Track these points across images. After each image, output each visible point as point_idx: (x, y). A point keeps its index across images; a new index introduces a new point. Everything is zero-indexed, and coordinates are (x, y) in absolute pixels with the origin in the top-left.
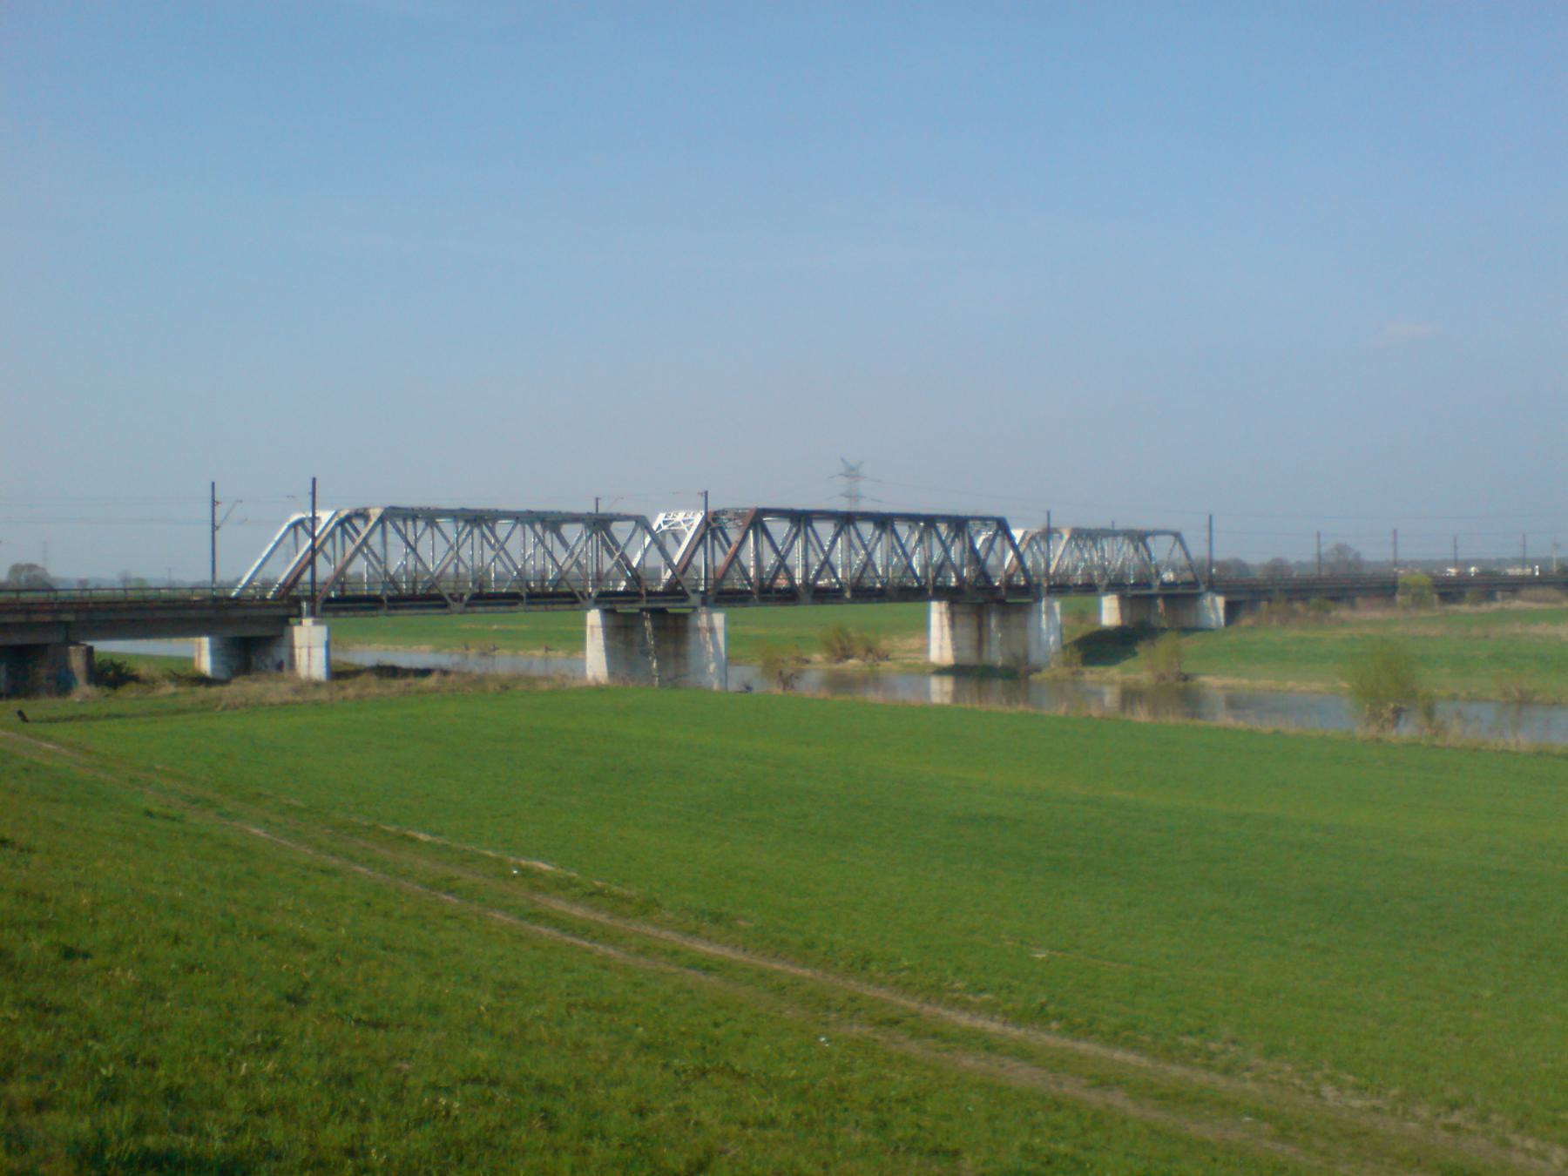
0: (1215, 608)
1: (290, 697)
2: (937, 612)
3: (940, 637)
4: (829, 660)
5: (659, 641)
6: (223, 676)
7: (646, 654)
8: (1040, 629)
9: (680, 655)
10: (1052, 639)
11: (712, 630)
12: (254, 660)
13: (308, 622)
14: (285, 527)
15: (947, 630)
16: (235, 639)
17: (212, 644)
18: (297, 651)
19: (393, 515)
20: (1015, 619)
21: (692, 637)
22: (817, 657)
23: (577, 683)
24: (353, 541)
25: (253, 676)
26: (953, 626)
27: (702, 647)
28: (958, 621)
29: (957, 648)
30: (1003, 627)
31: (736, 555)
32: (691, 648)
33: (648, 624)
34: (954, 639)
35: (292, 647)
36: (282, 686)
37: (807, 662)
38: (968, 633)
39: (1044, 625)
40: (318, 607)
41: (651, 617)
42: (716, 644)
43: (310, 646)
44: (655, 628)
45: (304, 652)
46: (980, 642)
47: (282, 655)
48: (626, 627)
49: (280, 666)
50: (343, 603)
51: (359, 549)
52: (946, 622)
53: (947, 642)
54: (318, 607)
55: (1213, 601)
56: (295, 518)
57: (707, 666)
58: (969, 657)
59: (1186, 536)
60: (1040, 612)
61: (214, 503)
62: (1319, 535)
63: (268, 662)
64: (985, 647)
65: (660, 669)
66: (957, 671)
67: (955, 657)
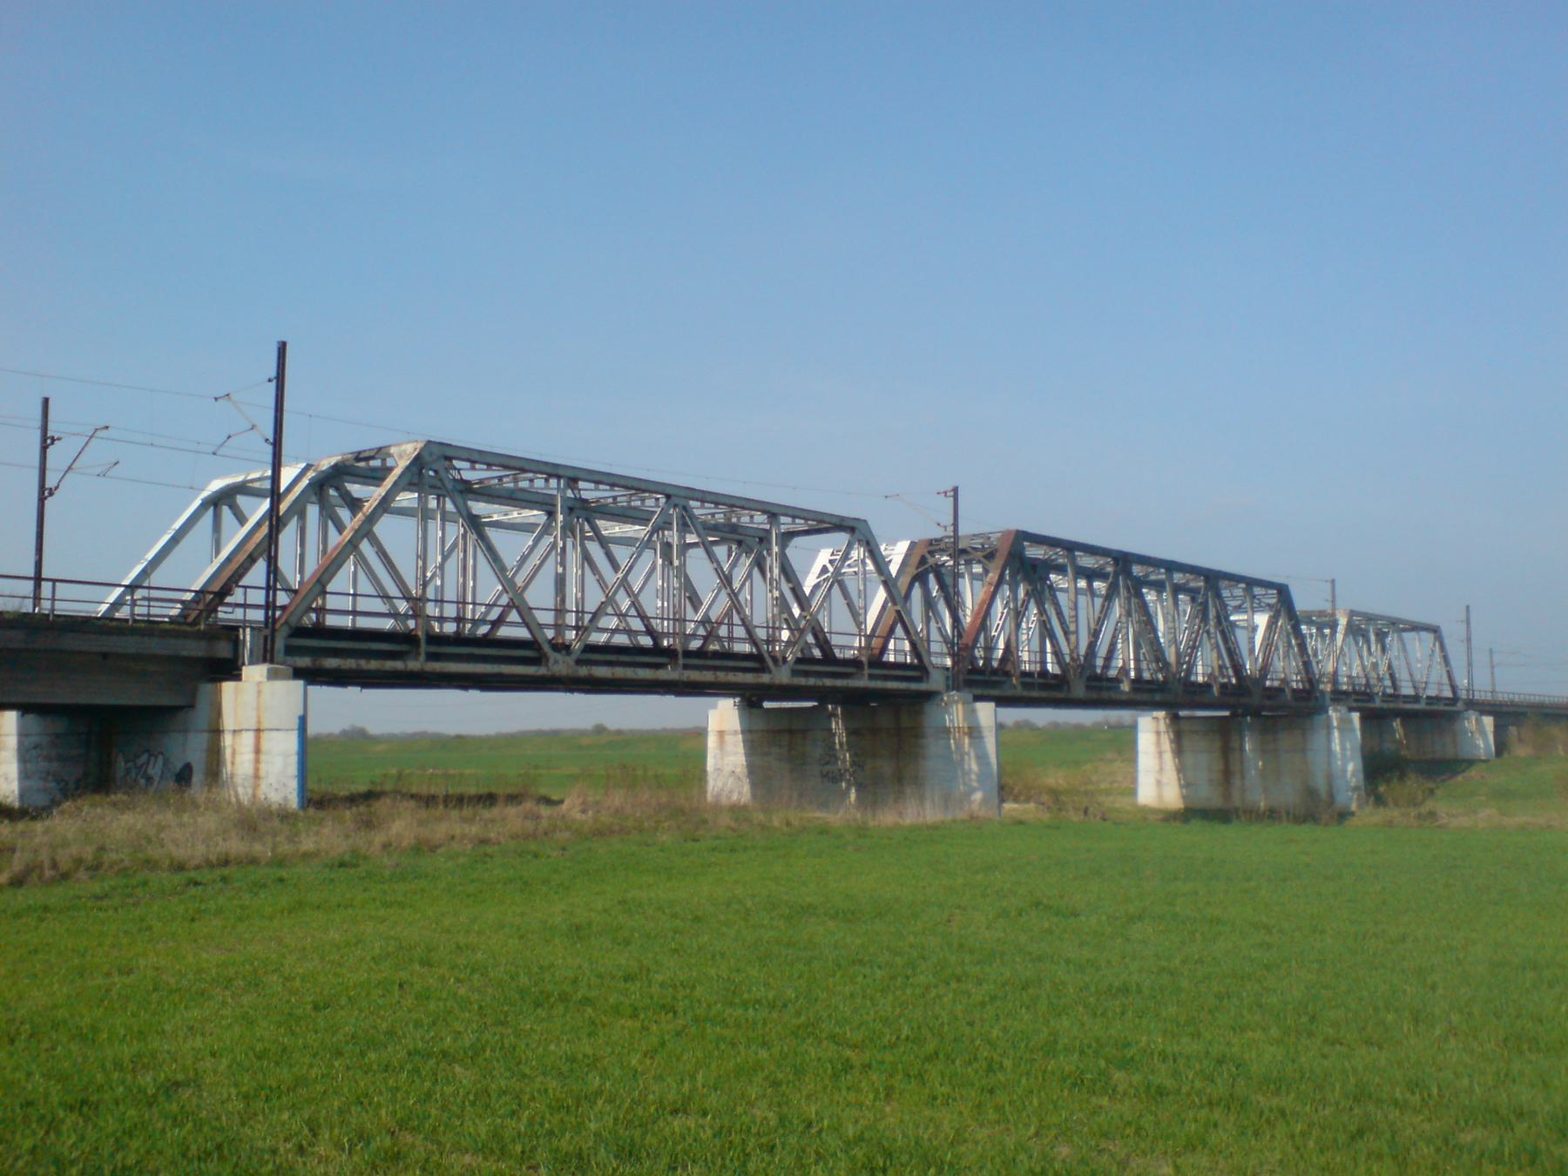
0: (1483, 733)
1: (235, 845)
2: (1150, 733)
3: (1155, 768)
6: (41, 800)
7: (835, 778)
8: (1329, 751)
10: (1350, 767)
11: (974, 732)
12: (121, 765)
13: (254, 673)
14: (198, 502)
15: (1168, 757)
17: (22, 735)
18: (227, 740)
19: (434, 471)
20: (1285, 740)
21: (932, 746)
23: (1121, 803)
24: (340, 528)
25: (120, 797)
26: (1178, 751)
28: (1186, 743)
29: (1186, 784)
30: (1263, 751)
33: (837, 726)
34: (1180, 770)
35: (216, 731)
36: (208, 821)
38: (1205, 759)
40: (280, 644)
41: (847, 712)
42: (982, 758)
43: (262, 727)
44: (851, 732)
45: (248, 739)
47: (192, 750)
48: (791, 732)
49: (184, 776)
50: (322, 652)
51: (352, 546)
53: (1171, 775)
54: (280, 644)
55: (1478, 722)
56: (217, 485)
58: (1209, 795)
59: (1445, 631)
60: (1329, 727)
61: (46, 441)
62: (1491, 651)
63: (155, 770)
64: (1237, 782)
67: (1184, 797)
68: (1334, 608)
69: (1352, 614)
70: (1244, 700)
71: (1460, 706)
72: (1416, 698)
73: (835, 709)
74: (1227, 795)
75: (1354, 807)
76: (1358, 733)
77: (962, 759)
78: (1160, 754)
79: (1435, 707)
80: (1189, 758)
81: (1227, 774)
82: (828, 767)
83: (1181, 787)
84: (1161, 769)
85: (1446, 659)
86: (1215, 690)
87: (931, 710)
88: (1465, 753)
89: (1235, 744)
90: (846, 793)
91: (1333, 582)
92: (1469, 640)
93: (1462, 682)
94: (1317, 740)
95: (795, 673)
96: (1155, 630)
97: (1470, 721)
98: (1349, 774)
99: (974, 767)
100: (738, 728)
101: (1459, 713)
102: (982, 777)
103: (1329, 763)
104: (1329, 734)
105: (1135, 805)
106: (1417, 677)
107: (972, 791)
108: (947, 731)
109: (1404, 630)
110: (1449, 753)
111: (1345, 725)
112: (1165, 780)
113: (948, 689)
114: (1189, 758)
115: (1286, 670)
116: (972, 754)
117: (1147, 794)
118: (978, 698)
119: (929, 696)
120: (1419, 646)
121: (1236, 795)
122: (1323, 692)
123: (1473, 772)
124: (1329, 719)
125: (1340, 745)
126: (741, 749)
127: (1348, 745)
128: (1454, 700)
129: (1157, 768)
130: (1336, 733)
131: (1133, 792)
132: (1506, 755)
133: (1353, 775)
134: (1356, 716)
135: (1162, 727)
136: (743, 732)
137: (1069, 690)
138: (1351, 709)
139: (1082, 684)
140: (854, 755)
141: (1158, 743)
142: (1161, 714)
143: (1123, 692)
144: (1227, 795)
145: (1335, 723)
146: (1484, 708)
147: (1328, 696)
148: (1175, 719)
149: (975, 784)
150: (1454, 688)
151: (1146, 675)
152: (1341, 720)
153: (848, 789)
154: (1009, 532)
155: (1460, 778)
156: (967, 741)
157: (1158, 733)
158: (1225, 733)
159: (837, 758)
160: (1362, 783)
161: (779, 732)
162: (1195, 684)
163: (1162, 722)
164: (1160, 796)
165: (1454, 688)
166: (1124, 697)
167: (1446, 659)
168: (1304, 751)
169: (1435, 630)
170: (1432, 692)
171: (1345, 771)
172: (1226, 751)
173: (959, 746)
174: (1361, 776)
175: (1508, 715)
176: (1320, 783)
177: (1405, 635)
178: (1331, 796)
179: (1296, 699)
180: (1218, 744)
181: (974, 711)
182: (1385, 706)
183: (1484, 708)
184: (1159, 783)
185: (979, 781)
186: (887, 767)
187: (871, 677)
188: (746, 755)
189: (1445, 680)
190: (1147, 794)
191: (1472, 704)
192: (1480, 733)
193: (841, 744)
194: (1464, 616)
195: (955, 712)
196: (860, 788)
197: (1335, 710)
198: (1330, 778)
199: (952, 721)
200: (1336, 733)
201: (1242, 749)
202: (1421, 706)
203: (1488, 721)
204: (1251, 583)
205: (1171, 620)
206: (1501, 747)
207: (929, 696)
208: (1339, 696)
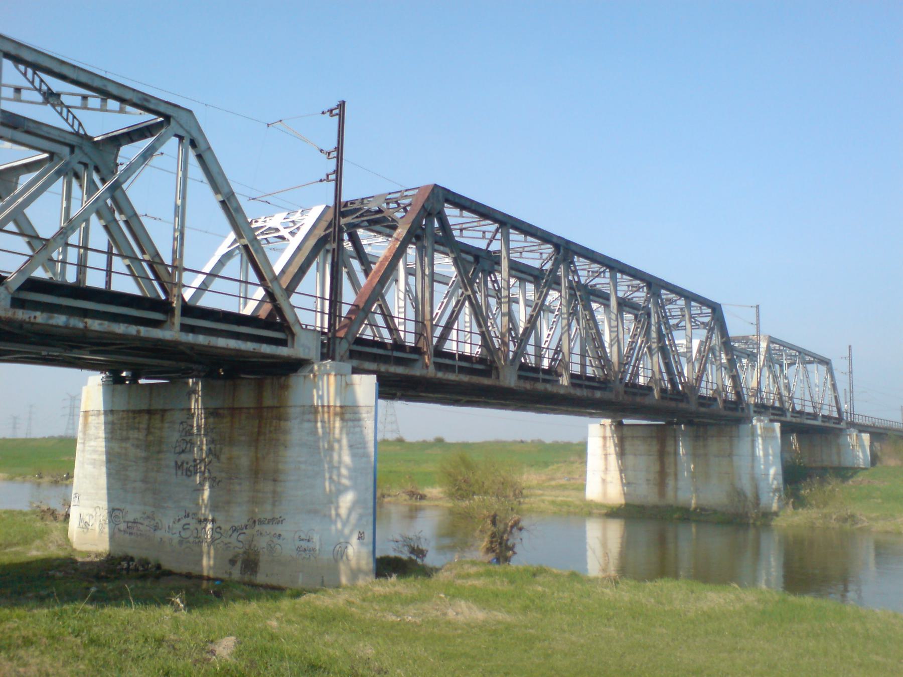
0: (862, 446)
4: (451, 496)
5: (218, 441)
7: (190, 473)
9: (264, 475)
10: (772, 471)
15: (613, 459)
16: (878, 564)
20: (714, 446)
21: (296, 431)
22: (434, 491)
26: (622, 454)
27: (319, 451)
29: (627, 483)
30: (694, 455)
31: (377, 294)
32: (294, 456)
37: (423, 497)
38: (644, 461)
39: (760, 452)
44: (211, 413)
46: (662, 478)
52: (612, 449)
53: (614, 475)
57: (332, 499)
58: (647, 494)
59: (834, 364)
60: (753, 434)
64: (670, 482)
65: (214, 506)
66: (628, 513)
67: (625, 499)
68: (758, 334)
69: (772, 340)
70: (683, 405)
71: (843, 425)
72: (814, 416)
73: (196, 384)
74: (662, 492)
75: (775, 507)
76: (779, 441)
77: (331, 448)
78: (606, 455)
79: (827, 424)
80: (630, 460)
81: (662, 475)
82: (183, 457)
83: (623, 485)
84: (606, 469)
85: (834, 386)
86: (656, 394)
87: (297, 381)
88: (847, 462)
89: (670, 449)
90: (199, 489)
91: (758, 307)
92: (851, 372)
93: (845, 407)
94: (743, 447)
95: (17, 303)
96: (599, 334)
97: (852, 437)
98: (771, 477)
99: (347, 459)
100: (102, 408)
101: (841, 430)
102: (355, 472)
103: (753, 468)
104: (753, 442)
105: (583, 500)
106: (816, 399)
107: (341, 490)
108: (314, 410)
109: (810, 362)
110: (835, 462)
111: (767, 435)
112: (609, 479)
113: (324, 357)
114: (630, 460)
115: (715, 381)
116: (345, 442)
117: (594, 491)
118: (356, 371)
119: (296, 365)
120: (817, 373)
121: (670, 493)
122: (748, 405)
123: (859, 478)
124: (754, 428)
125: (762, 453)
126: (102, 434)
127: (771, 451)
128: (839, 420)
129: (603, 468)
130: (760, 440)
131: (582, 488)
132: (878, 465)
133: (774, 479)
134: (777, 426)
135: (608, 433)
136: (106, 413)
137: (498, 377)
138: (772, 421)
139: (536, 391)
140: (212, 442)
141: (605, 446)
142: (608, 422)
143: (562, 386)
144: (662, 492)
145: (759, 432)
146: (862, 429)
147: (752, 409)
148: (619, 425)
149: (345, 481)
150: (839, 410)
151: (590, 371)
152: (765, 429)
153: (202, 484)
154: (428, 186)
155: (850, 482)
156: (338, 424)
157: (605, 438)
158: (662, 439)
159: (193, 444)
160: (781, 486)
161: (140, 412)
162: (635, 386)
163: (608, 428)
164: (605, 494)
165: (839, 410)
166: (562, 391)
167: (834, 386)
168: (730, 455)
169: (825, 362)
170: (826, 413)
171: (767, 475)
172: (662, 455)
173: (328, 432)
174: (780, 479)
175: (879, 434)
176: (746, 485)
177: (809, 366)
178: (757, 498)
179: (725, 408)
180: (655, 448)
181: (349, 385)
182: (794, 420)
183: (862, 429)
184: (604, 481)
185: (350, 478)
186: (243, 457)
187: (185, 328)
188: (108, 440)
189: (834, 404)
190: (594, 491)
191: (852, 424)
192: (859, 448)
193: (199, 427)
194: (847, 354)
195: (325, 386)
196: (215, 483)
197: (759, 420)
198: (754, 479)
199: (321, 397)
200: (760, 440)
201: (676, 453)
202: (818, 423)
203: (866, 437)
204: (689, 297)
205: (615, 331)
206: (875, 459)
207: (296, 365)
208: (762, 409)
